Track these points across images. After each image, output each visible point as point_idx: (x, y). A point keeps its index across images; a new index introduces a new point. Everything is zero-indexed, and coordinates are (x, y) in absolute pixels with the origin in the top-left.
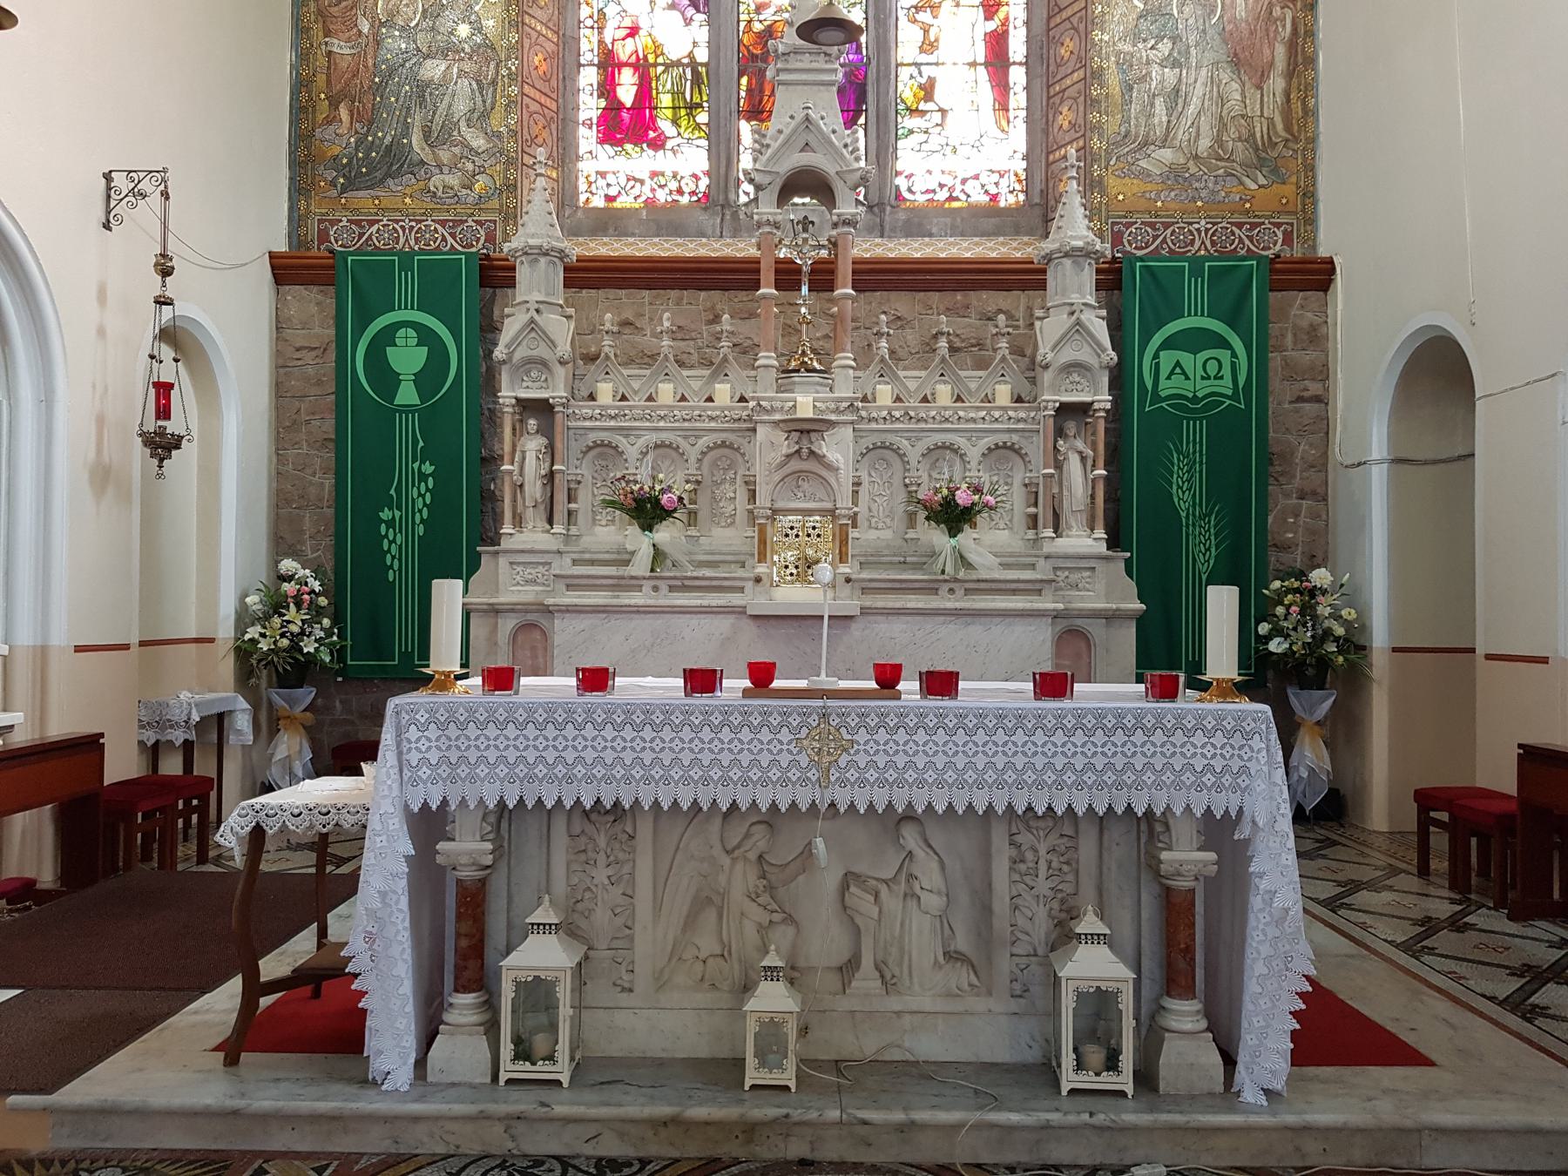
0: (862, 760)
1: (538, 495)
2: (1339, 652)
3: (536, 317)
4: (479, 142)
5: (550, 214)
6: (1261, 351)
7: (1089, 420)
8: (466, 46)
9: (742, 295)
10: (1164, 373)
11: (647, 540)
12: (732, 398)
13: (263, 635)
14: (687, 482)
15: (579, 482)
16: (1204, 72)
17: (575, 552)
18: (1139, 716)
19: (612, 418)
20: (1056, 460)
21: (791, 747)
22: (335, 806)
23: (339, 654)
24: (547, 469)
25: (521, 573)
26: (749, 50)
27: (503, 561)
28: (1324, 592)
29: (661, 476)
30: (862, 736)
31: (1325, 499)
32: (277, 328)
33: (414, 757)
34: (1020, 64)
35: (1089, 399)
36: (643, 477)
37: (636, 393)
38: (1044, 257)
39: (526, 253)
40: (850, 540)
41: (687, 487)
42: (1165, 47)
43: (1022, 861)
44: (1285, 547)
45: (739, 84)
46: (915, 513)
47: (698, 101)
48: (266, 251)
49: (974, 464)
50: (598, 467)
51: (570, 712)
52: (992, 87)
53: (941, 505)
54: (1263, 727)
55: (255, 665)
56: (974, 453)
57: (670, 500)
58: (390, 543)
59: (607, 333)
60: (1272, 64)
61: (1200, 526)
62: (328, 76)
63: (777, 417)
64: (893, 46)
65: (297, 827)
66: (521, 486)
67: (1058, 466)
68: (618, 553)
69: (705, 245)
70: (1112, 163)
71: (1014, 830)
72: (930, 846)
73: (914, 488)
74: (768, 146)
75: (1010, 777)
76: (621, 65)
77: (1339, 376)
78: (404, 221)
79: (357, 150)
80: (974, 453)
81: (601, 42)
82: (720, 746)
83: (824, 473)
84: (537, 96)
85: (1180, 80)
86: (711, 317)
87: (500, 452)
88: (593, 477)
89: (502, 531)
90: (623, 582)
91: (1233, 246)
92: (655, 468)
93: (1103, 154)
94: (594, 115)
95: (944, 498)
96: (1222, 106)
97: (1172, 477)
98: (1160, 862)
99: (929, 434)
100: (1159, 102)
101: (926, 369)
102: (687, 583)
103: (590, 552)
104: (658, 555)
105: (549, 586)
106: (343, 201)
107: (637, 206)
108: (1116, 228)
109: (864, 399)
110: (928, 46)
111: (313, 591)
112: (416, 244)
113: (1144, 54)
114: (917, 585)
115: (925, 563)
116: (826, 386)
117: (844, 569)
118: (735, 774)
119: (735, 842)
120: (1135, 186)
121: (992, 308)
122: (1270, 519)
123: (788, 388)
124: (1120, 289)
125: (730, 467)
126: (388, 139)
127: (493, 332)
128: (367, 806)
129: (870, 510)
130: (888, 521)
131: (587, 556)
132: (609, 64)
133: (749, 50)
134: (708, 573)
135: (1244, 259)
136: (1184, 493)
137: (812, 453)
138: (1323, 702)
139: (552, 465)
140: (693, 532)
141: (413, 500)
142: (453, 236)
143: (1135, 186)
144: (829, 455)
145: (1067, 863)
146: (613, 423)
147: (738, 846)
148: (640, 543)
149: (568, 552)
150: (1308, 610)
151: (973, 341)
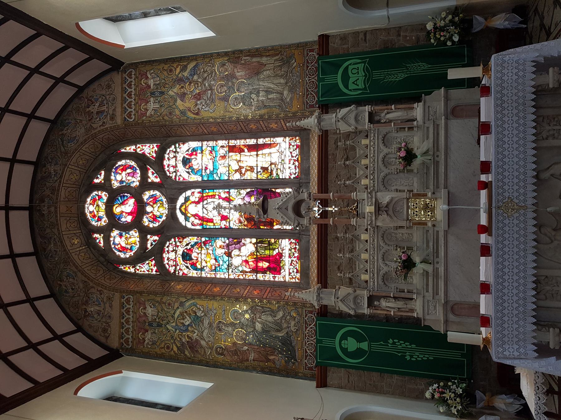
0: (516, 194)
1: (402, 303)
2: (458, 16)
3: (340, 299)
4: (281, 314)
5: (306, 292)
6: (348, 55)
7: (374, 112)
8: (252, 315)
9: (329, 229)
10: (356, 87)
11: (419, 265)
12: (366, 234)
13: (455, 407)
14: (396, 250)
15: (397, 288)
16: (261, 83)
17: (424, 292)
18: (496, 99)
19: (374, 275)
20: (388, 122)
21: (511, 219)
22: (535, 384)
23: (462, 380)
24: (392, 299)
25: (432, 311)
26: (253, 226)
27: (427, 317)
28: (435, 24)
29: (395, 259)
30: (507, 194)
31: (400, 27)
32: (341, 388)
33: (516, 354)
34: (257, 141)
35: (367, 113)
36: (394, 265)
37: (364, 266)
38: (320, 131)
39: (319, 301)
40: (418, 193)
41: (399, 250)
42: (253, 96)
43: (554, 135)
44: (418, 39)
45: (263, 229)
46: (407, 170)
47: (268, 242)
48: (316, 389)
49: (389, 150)
50: (391, 281)
51: (498, 298)
52: (264, 149)
53: (405, 161)
54: (500, 57)
55: (467, 412)
56: (386, 150)
57: (404, 256)
58: (418, 357)
59: (344, 275)
60: (258, 62)
61: (411, 69)
62: (261, 361)
63: (374, 218)
64: (252, 181)
65: (544, 399)
66: (399, 308)
67: (390, 121)
68: (424, 276)
69: (312, 241)
70: (288, 110)
71: (541, 138)
72: (548, 168)
73: (398, 170)
74: (286, 221)
75: (521, 142)
76: (257, 266)
77: (357, 28)
78: (306, 341)
79: (283, 354)
80: (386, 150)
81: (250, 272)
82: (511, 245)
83: (394, 202)
84: (266, 294)
85: (263, 91)
86: (336, 239)
87: (384, 315)
88: (395, 283)
89: (416, 317)
90: (435, 275)
91: (314, 68)
92: (392, 261)
93: (285, 113)
94: (272, 275)
95: (403, 160)
96: (271, 76)
97: (393, 81)
98: (553, 87)
99: (379, 166)
100: (270, 97)
101: (356, 168)
102: (435, 251)
103: (424, 286)
104: (424, 261)
105: (437, 301)
106: (299, 361)
107: (300, 263)
108: (308, 107)
109: (367, 188)
110: (252, 169)
111: (438, 387)
112: (313, 337)
113: (255, 102)
114: (436, 168)
115: (427, 166)
116: (362, 202)
117: (429, 194)
118: (522, 240)
119: (548, 239)
120: (295, 102)
121: (334, 146)
122: (408, 45)
123: (363, 215)
124: (328, 104)
125: (391, 235)
126: (280, 344)
127: (342, 314)
128: (535, 372)
129: (406, 186)
130: (410, 179)
131: (425, 287)
132: (256, 270)
133: (253, 226)
134: (431, 244)
135: (319, 64)
136: (398, 76)
137: (386, 207)
138: (478, 20)
139: (391, 297)
140: (415, 249)
141: (403, 347)
142: (310, 325)
143: (295, 102)
144: (387, 200)
145: (554, 119)
146: (376, 275)
147: (550, 238)
148: (420, 268)
149: (424, 293)
150: (442, 29)
151: (345, 151)
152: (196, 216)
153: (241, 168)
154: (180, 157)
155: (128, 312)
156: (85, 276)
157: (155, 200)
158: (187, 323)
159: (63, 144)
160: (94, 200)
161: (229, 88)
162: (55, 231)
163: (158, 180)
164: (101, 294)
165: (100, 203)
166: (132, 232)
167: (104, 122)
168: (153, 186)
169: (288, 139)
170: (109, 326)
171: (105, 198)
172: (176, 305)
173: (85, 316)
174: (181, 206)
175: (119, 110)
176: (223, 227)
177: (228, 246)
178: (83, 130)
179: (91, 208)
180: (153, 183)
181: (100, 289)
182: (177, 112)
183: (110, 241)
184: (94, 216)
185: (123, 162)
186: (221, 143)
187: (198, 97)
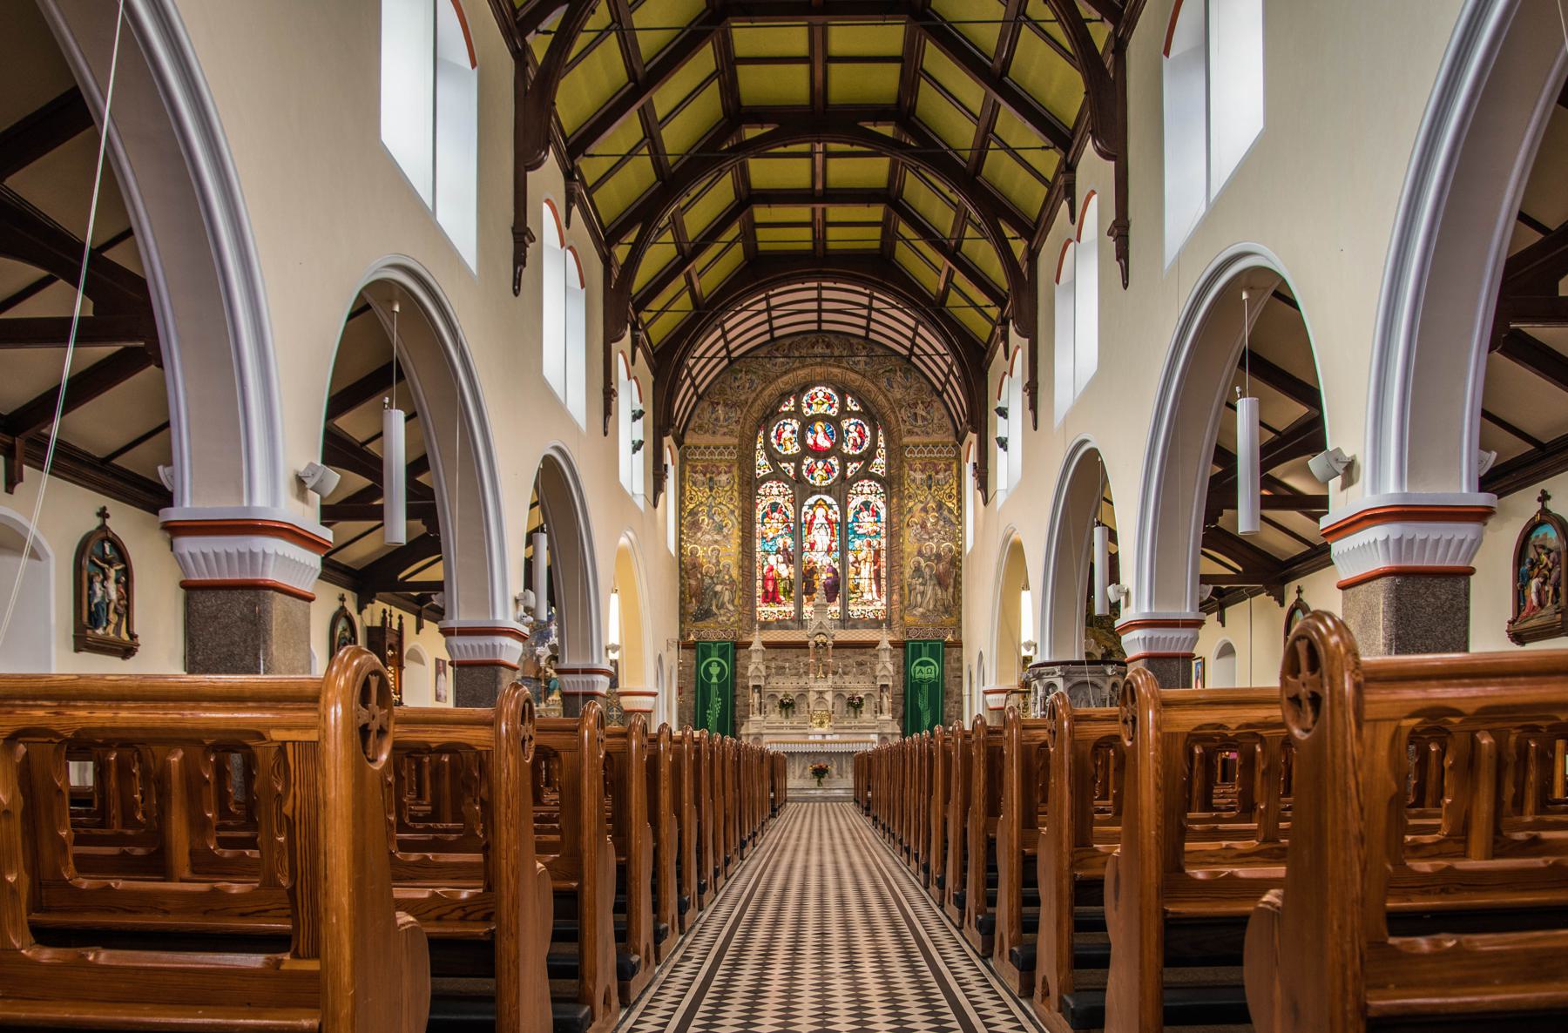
4: (731, 608)
100: (919, 596)
110: (858, 573)
120: (912, 619)
132: (765, 579)
152: (814, 516)
153: (859, 563)
154: (872, 498)
155: (721, 454)
157: (829, 471)
160: (829, 398)
161: (930, 557)
163: (849, 474)
165: (826, 406)
166: (797, 446)
168: (844, 469)
169: (884, 608)
170: (705, 433)
171: (830, 412)
172: (731, 507)
173: (712, 403)
174: (825, 502)
175: (916, 439)
177: (786, 550)
178: (899, 396)
179: (821, 395)
181: (741, 420)
182: (911, 504)
183: (786, 418)
184: (812, 399)
185: (868, 433)
186: (883, 541)
187: (923, 526)
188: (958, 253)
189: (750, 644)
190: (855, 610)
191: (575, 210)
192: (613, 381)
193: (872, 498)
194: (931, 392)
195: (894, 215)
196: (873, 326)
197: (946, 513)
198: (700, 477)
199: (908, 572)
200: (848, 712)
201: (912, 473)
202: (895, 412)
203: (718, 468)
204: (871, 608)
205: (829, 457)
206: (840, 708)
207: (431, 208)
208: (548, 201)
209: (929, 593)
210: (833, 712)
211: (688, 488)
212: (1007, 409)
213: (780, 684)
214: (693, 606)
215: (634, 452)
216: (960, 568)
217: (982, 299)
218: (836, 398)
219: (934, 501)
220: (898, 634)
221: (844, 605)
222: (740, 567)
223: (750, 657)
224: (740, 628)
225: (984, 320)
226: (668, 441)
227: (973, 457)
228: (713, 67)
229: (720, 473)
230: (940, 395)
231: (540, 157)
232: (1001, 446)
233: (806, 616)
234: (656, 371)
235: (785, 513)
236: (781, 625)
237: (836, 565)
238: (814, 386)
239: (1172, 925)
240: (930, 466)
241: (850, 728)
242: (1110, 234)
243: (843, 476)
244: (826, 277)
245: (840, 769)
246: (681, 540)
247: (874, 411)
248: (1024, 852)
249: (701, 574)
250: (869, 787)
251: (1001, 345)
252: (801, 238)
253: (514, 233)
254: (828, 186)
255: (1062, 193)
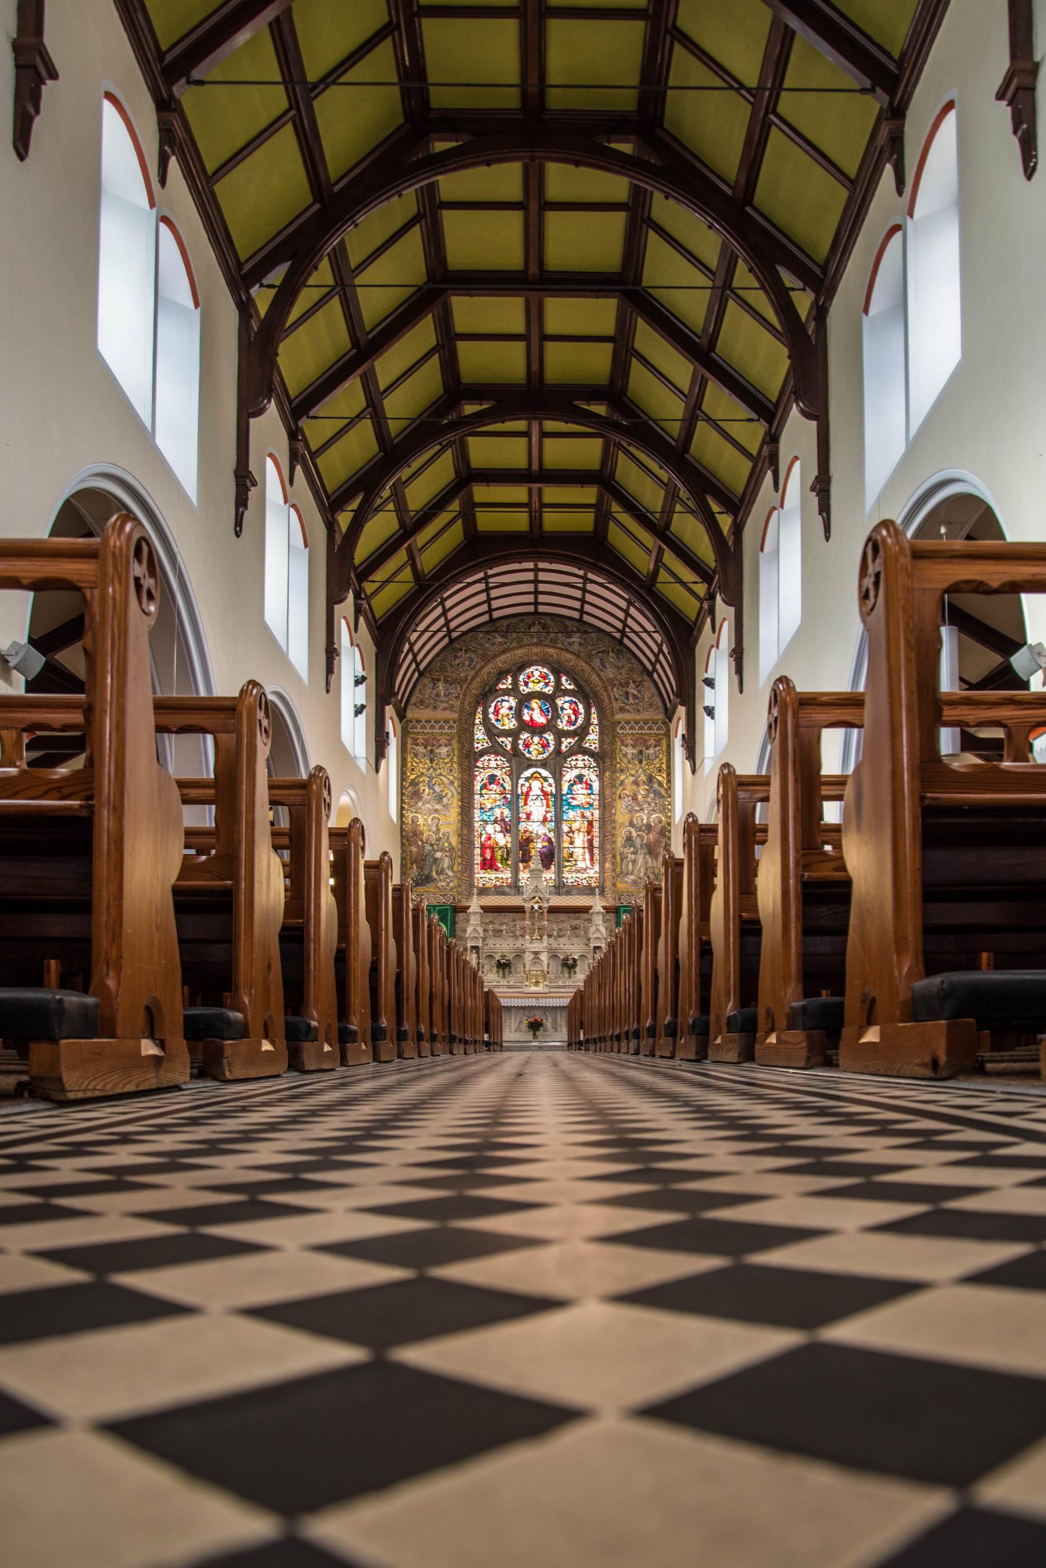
4: (450, 874)
76: (487, 848)
94: (479, 862)
100: (630, 864)
110: (572, 843)
132: (483, 847)
152: (530, 788)
153: (573, 832)
154: (585, 772)
155: (441, 727)
156: (472, 680)
157: (545, 746)
158: (435, 788)
159: (599, 652)
160: (545, 677)
161: (640, 827)
162: (514, 644)
163: (563, 748)
164: (456, 698)
165: (542, 684)
166: (514, 721)
167: (617, 700)
168: (559, 743)
169: (597, 875)
170: (427, 707)
171: (546, 690)
172: (451, 778)
173: (433, 679)
174: (540, 774)
176: (520, 815)
177: (503, 820)
178: (611, 676)
179: (537, 674)
180: (561, 743)
181: (461, 696)
182: (622, 777)
183: (504, 696)
184: (529, 677)
185: (582, 710)
186: (596, 813)
187: (634, 798)
188: (667, 532)
189: (468, 907)
190: (570, 877)
191: (298, 468)
192: (336, 641)
193: (585, 772)
194: (642, 672)
195: (607, 496)
196: (587, 608)
197: (656, 786)
198: (421, 749)
199: (620, 842)
200: (562, 972)
201: (623, 747)
202: (607, 691)
203: (438, 740)
204: (584, 876)
205: (545, 732)
206: (554, 970)
207: (150, 430)
208: (271, 455)
209: (640, 861)
210: (548, 973)
211: (409, 759)
212: (713, 680)
213: (498, 946)
214: (414, 871)
215: (356, 715)
216: (669, 838)
217: (687, 574)
218: (552, 677)
219: (645, 775)
220: (610, 900)
221: (559, 872)
222: (459, 835)
223: (468, 921)
224: (459, 893)
225: (691, 597)
226: (389, 711)
227: (682, 729)
228: (434, 342)
229: (440, 746)
230: (650, 675)
231: (262, 405)
232: (709, 715)
233: (522, 882)
234: (379, 642)
235: (502, 785)
236: (498, 890)
237: (551, 835)
238: (532, 665)
239: (929, 812)
240: (641, 742)
241: (564, 987)
242: (812, 489)
243: (558, 751)
244: (542, 557)
245: (555, 1022)
246: (402, 808)
247: (588, 690)
248: (741, 916)
249: (422, 841)
250: (582, 1023)
251: (709, 620)
252: (520, 521)
253: (236, 476)
254: (544, 467)
255: (767, 464)
